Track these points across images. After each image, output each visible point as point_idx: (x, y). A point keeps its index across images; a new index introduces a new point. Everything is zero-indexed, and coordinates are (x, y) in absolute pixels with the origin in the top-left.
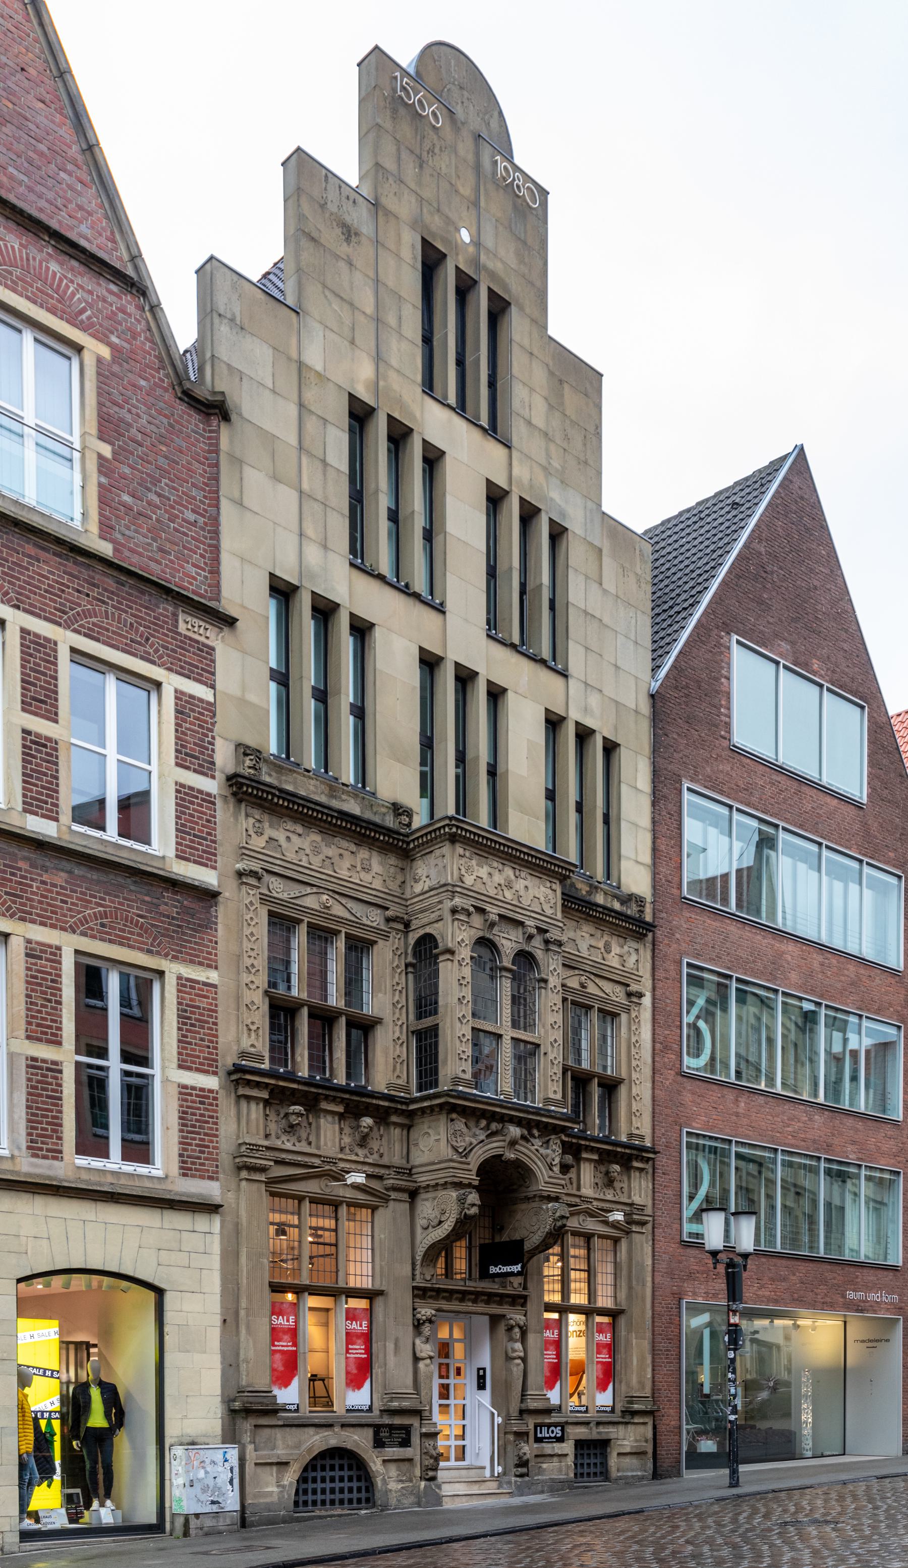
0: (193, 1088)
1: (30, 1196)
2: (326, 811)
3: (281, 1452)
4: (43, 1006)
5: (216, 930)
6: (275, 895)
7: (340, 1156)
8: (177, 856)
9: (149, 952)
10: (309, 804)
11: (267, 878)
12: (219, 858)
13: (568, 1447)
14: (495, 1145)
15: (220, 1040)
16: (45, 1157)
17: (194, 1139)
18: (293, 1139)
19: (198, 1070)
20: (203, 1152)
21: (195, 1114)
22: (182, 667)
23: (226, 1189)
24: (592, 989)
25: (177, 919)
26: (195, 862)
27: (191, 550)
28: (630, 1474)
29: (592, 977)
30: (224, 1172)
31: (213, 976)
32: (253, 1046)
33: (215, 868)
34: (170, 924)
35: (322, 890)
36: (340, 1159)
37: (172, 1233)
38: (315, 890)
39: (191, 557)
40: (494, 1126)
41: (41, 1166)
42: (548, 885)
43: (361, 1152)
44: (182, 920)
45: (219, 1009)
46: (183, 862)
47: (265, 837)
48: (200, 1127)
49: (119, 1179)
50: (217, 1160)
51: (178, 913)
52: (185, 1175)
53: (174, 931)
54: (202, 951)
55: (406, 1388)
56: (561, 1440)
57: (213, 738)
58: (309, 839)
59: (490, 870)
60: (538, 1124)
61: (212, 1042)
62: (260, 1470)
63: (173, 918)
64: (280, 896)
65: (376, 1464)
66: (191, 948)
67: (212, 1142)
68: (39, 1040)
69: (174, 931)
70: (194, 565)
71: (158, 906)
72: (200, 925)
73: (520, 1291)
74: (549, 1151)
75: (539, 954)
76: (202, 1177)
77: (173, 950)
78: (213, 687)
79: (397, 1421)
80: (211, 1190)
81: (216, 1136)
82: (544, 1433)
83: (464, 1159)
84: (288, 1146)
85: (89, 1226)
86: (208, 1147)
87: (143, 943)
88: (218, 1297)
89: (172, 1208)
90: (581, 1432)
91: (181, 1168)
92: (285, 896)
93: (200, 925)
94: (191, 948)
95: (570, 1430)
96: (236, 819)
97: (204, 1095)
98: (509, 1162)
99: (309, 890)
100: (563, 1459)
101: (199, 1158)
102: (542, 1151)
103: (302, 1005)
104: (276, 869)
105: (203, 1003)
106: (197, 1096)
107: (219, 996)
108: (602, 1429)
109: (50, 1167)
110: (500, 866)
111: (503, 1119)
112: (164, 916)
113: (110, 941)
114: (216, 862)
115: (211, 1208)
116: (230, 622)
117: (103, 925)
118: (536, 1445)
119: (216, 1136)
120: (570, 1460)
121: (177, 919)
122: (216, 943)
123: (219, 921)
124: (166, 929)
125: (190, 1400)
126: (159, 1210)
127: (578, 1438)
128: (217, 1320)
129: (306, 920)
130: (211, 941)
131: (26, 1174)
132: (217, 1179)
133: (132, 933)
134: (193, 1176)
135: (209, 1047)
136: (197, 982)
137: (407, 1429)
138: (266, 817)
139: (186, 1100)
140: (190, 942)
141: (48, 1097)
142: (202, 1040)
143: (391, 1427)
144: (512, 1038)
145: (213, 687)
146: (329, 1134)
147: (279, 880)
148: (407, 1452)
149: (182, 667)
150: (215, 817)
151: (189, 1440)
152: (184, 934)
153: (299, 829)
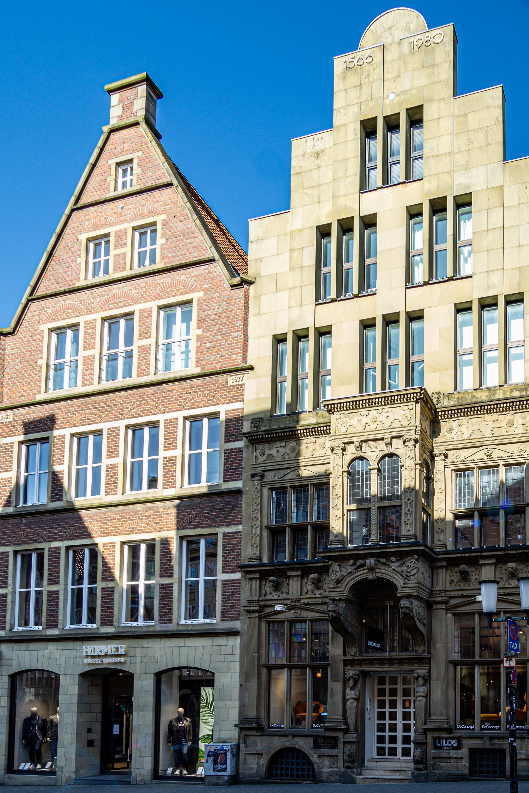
0: (229, 581)
1: (159, 639)
2: (289, 430)
3: (259, 748)
4: (166, 563)
5: (241, 507)
6: (270, 480)
7: (301, 597)
8: (224, 481)
9: (211, 527)
10: (280, 431)
11: (267, 474)
12: (243, 475)
13: (464, 752)
14: (361, 573)
15: (243, 555)
16: (166, 623)
17: (229, 603)
18: (278, 594)
19: (231, 572)
20: (233, 608)
21: (229, 592)
22: (229, 400)
23: (243, 623)
24: (496, 453)
25: (223, 508)
26: (232, 480)
27: (234, 348)
28: (525, 774)
29: (496, 447)
30: (243, 616)
31: (240, 528)
32: (254, 554)
33: (241, 479)
34: (219, 512)
35: (296, 468)
36: (301, 598)
37: (217, 647)
38: (292, 469)
39: (234, 351)
40: (360, 562)
41: (164, 627)
42: (406, 408)
43: (318, 592)
44: (225, 508)
45: (242, 542)
46: (227, 483)
47: (266, 455)
48: (232, 597)
49: (194, 627)
50: (239, 611)
51: (223, 506)
52: (224, 620)
53: (222, 514)
54: (235, 518)
55: (338, 715)
56: (458, 748)
57: (242, 423)
58: (289, 447)
59: (359, 418)
60: (394, 554)
61: (238, 557)
62: (248, 756)
63: (221, 509)
64: (274, 479)
65: (314, 757)
66: (229, 519)
67: (237, 603)
68: (165, 576)
69: (222, 514)
70: (236, 354)
71: (214, 506)
72: (234, 507)
73: (426, 655)
74: (404, 568)
75: (399, 452)
76: (232, 620)
77: (221, 522)
78: (243, 401)
79: (328, 734)
80: (236, 625)
81: (239, 600)
82: (443, 743)
83: (338, 586)
84: (276, 597)
85: (182, 649)
86: (235, 606)
87: (208, 524)
88: (238, 674)
89: (216, 636)
90: (477, 743)
91: (222, 617)
92: (276, 478)
93: (234, 507)
94: (229, 519)
95: (464, 742)
96: (252, 453)
97: (234, 582)
98: (373, 581)
99: (289, 471)
100: (459, 761)
101: (231, 611)
102: (399, 569)
103: (499, 509)
104: (270, 468)
105: (234, 541)
106: (230, 584)
107: (243, 536)
108: (496, 741)
109: (167, 627)
110: (367, 413)
111: (365, 557)
112: (217, 509)
113: (194, 528)
114: (242, 476)
115: (234, 633)
116: (252, 368)
117: (191, 522)
118: (434, 751)
119: (239, 600)
120: (465, 763)
121: (223, 508)
122: (241, 512)
123: (243, 502)
124: (218, 514)
125: (223, 722)
126: (233, 637)
127: (472, 747)
128: (237, 685)
129: (288, 485)
130: (239, 513)
131: (159, 631)
132: (239, 620)
133: (203, 521)
134: (228, 620)
135: (237, 560)
136: (232, 533)
137: (336, 739)
138: (267, 446)
139: (225, 587)
140: (229, 516)
141: (167, 598)
142: (234, 558)
143: (325, 738)
144: (378, 508)
145: (243, 401)
146: (295, 587)
147: (272, 472)
148: (334, 752)
149: (229, 400)
150: (242, 457)
151: (222, 740)
152: (226, 514)
153: (283, 444)
